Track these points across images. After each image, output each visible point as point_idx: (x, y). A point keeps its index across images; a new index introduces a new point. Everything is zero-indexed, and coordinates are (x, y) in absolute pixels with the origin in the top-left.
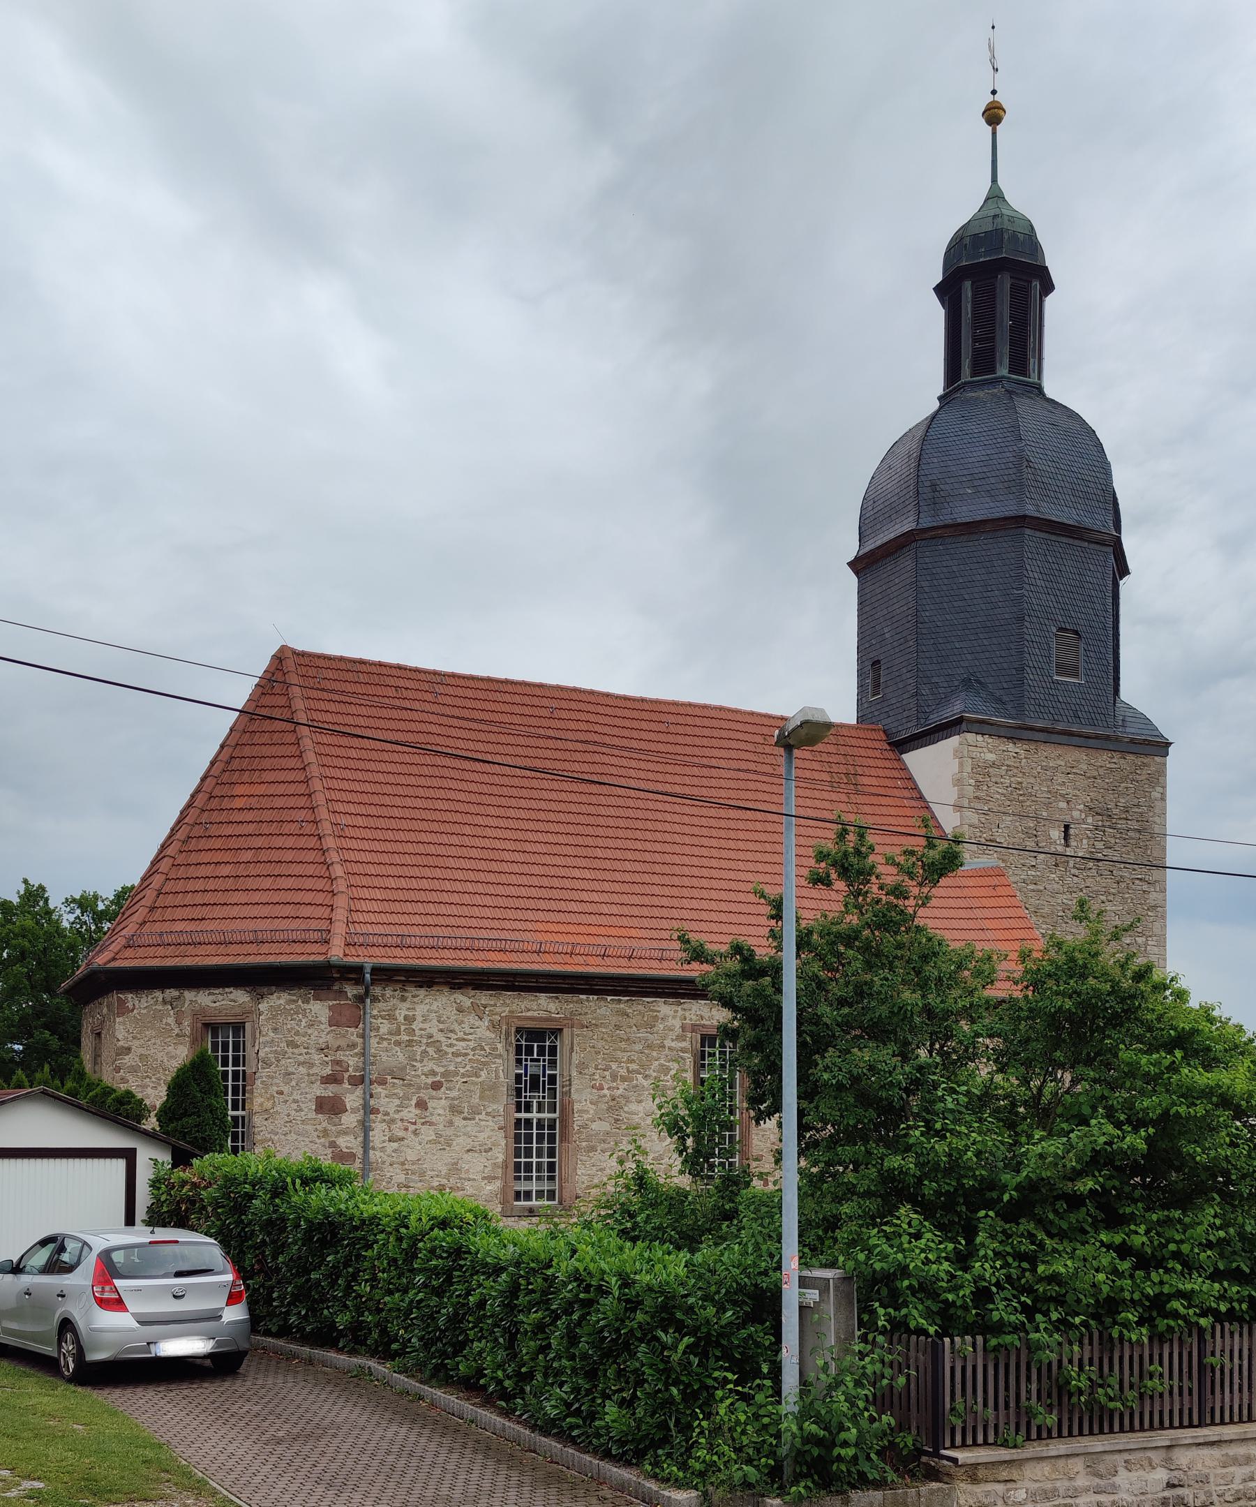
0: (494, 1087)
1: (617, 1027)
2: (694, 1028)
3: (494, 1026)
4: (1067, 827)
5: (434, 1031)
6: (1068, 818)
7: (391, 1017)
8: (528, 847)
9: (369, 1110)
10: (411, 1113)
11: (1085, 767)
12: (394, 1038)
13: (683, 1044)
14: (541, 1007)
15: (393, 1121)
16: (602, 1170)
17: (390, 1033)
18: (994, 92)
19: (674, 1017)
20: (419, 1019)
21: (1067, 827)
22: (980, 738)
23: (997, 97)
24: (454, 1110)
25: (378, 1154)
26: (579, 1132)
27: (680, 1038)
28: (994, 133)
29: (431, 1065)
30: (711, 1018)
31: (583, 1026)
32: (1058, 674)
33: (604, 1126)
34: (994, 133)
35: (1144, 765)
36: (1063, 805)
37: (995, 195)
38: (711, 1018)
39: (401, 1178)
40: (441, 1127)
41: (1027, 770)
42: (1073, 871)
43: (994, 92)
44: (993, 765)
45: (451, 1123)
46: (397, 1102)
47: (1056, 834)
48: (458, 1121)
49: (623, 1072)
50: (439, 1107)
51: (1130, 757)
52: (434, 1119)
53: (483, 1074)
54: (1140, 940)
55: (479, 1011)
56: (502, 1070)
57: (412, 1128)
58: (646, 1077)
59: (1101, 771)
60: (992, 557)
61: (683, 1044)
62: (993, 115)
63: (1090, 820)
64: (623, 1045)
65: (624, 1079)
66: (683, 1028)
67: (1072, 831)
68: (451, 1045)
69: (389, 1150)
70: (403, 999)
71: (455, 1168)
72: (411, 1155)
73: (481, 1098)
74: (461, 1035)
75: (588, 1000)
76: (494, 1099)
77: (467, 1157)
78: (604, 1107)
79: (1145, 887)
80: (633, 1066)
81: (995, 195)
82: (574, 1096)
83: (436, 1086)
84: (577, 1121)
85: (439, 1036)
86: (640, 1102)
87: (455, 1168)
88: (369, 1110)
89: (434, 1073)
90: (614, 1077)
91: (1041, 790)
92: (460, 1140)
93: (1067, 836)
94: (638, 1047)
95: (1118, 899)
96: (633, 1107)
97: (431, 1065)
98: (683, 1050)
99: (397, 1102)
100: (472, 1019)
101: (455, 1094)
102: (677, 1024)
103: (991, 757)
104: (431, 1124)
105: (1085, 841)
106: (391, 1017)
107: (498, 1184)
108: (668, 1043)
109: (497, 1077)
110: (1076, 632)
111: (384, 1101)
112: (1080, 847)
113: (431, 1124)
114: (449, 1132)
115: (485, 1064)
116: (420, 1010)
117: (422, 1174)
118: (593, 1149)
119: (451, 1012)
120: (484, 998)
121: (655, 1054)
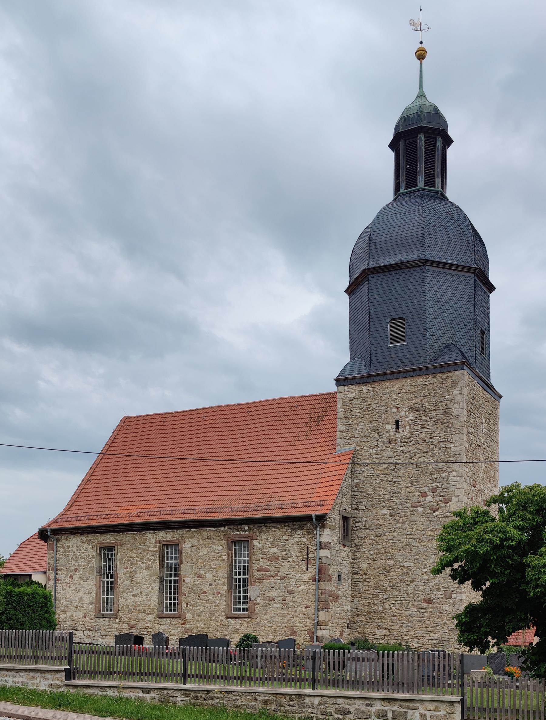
0: (92, 570)
1: (133, 544)
2: (160, 542)
3: (93, 547)
4: (397, 422)
5: (75, 550)
6: (398, 418)
7: (63, 547)
8: (189, 478)
9: (56, 579)
10: (68, 579)
11: (409, 388)
12: (64, 554)
13: (156, 549)
14: (108, 539)
15: (63, 583)
16: (127, 600)
17: (63, 552)
18: (421, 43)
19: (153, 538)
20: (71, 546)
21: (397, 422)
22: (346, 387)
23: (423, 45)
24: (81, 578)
25: (59, 595)
26: (119, 585)
27: (155, 547)
28: (421, 64)
29: (74, 563)
30: (167, 537)
31: (121, 545)
32: (391, 343)
33: (127, 583)
34: (421, 64)
35: (448, 377)
36: (395, 410)
37: (421, 95)
38: (167, 537)
39: (65, 603)
40: (77, 585)
41: (374, 397)
42: (400, 444)
43: (421, 43)
44: (354, 399)
45: (80, 583)
46: (64, 576)
47: (390, 427)
48: (82, 583)
49: (135, 562)
50: (76, 577)
51: (438, 376)
52: (75, 582)
53: (89, 565)
54: (443, 475)
55: (88, 541)
56: (95, 563)
57: (68, 585)
58: (143, 563)
59: (420, 388)
60: (417, 287)
61: (156, 549)
62: (421, 55)
63: (411, 415)
64: (135, 551)
65: (135, 564)
66: (156, 542)
67: (400, 423)
68: (80, 555)
69: (62, 593)
70: (67, 540)
71: (81, 599)
72: (68, 595)
73: (89, 574)
74: (83, 551)
75: (123, 535)
76: (92, 574)
77: (84, 595)
78: (128, 575)
79: (448, 445)
80: (138, 559)
81: (421, 95)
82: (118, 572)
83: (76, 570)
84: (119, 581)
85: (77, 552)
86: (140, 573)
87: (81, 599)
88: (56, 579)
89: (75, 565)
90: (131, 564)
91: (381, 406)
92: (82, 589)
93: (397, 427)
94: (140, 551)
95: (429, 454)
96: (138, 575)
97: (74, 563)
98: (156, 551)
99: (64, 576)
100: (86, 545)
101: (80, 573)
102: (154, 541)
103: (352, 395)
104: (74, 584)
105: (408, 427)
106: (63, 547)
107: (94, 605)
108: (150, 549)
109: (94, 566)
110: (402, 318)
111: (61, 576)
112: (405, 431)
113: (74, 584)
114: (79, 586)
115: (90, 561)
116: (72, 543)
117: (71, 602)
118: (124, 592)
119: (80, 543)
120: (90, 537)
121: (146, 554)
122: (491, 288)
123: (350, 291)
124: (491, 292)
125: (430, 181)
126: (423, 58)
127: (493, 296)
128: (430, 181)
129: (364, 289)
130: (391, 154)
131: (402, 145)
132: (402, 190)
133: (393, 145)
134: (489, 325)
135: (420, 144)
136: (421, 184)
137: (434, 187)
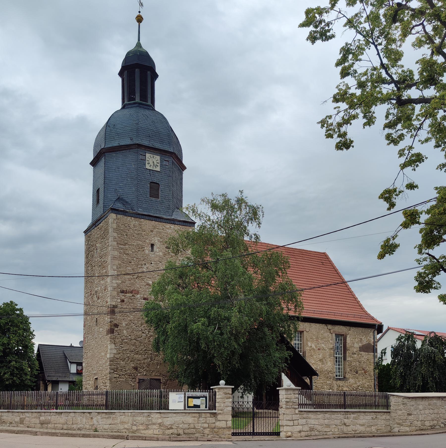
23: (141, 14)
28: (139, 40)
34: (139, 40)
37: (139, 45)
62: (140, 19)
81: (139, 45)
122: (184, 168)
123: (94, 163)
124: (183, 171)
125: (144, 97)
126: (141, 22)
127: (185, 173)
128: (144, 97)
129: (102, 164)
130: (120, 80)
131: (126, 72)
132: (126, 102)
133: (121, 74)
134: (182, 194)
135: (138, 74)
136: (138, 100)
137: (146, 102)
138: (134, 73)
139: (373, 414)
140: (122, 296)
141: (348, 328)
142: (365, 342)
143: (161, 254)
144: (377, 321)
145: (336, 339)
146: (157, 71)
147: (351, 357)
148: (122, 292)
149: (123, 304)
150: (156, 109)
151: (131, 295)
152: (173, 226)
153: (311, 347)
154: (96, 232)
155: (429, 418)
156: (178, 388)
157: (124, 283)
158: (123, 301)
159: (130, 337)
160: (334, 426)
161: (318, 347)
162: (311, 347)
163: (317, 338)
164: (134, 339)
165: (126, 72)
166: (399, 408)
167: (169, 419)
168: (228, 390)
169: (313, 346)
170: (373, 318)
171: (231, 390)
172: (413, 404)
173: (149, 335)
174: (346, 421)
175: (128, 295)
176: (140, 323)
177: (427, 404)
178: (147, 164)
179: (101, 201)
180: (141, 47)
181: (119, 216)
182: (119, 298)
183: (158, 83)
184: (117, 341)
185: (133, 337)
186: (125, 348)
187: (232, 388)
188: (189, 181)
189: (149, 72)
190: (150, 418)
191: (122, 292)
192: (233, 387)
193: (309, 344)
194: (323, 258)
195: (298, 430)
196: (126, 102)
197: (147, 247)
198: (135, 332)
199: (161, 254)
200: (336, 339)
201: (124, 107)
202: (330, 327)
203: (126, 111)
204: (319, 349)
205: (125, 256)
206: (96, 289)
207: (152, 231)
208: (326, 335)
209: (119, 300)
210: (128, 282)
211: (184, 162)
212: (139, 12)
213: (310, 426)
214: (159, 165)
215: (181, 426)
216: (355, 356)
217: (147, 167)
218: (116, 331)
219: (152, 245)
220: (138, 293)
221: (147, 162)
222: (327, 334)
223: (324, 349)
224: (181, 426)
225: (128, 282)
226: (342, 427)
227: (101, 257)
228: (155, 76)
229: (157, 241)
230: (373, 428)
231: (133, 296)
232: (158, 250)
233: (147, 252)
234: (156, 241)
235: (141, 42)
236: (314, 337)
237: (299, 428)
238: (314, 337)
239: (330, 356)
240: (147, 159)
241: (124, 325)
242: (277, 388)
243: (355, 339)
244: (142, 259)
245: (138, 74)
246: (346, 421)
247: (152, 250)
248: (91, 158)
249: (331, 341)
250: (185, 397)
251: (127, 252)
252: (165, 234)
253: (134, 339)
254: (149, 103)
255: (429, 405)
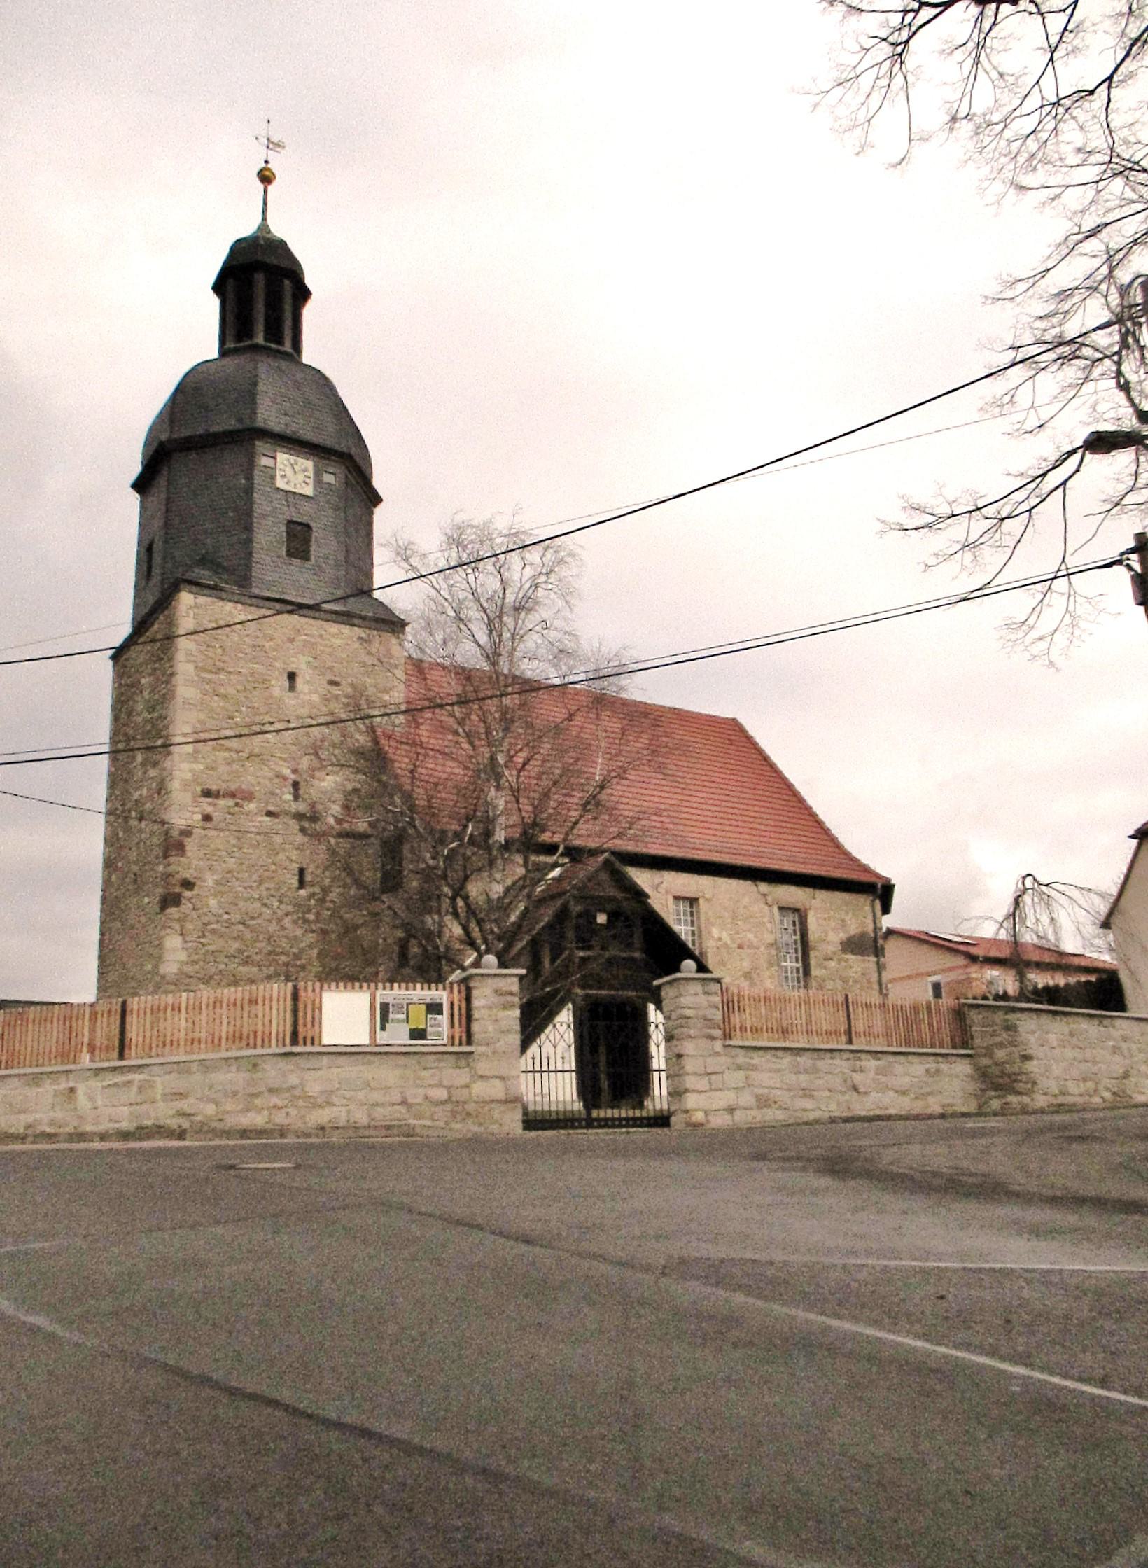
28: (264, 219)
34: (264, 219)
37: (264, 227)
62: (266, 177)
81: (264, 227)
122: (375, 499)
123: (141, 485)
125: (274, 332)
128: (274, 332)
129: (162, 481)
130: (214, 303)
133: (218, 288)
135: (261, 288)
136: (260, 339)
138: (250, 284)
139: (931, 1059)
140: (206, 805)
141: (809, 891)
142: (853, 929)
143: (315, 698)
144: (878, 876)
145: (782, 922)
146: (309, 281)
147: (820, 966)
148: (207, 793)
149: (208, 825)
150: (306, 359)
151: (231, 802)
152: (346, 630)
153: (720, 939)
154: (138, 655)
155: (1075, 1073)
156: (351, 978)
157: (213, 769)
158: (207, 818)
159: (226, 916)
160: (827, 1093)
161: (739, 941)
162: (720, 939)
163: (735, 917)
164: (239, 923)
165: (231, 283)
166: (998, 1039)
167: (320, 1073)
168: (510, 980)
169: (726, 937)
170: (866, 869)
171: (516, 980)
172: (1033, 1027)
173: (280, 913)
174: (858, 1078)
175: (222, 802)
176: (255, 877)
177: (1066, 1030)
178: (278, 477)
179: (156, 571)
180: (270, 232)
181: (202, 600)
182: (197, 809)
183: (309, 313)
184: (189, 926)
185: (236, 917)
186: (211, 948)
187: (521, 978)
188: (385, 522)
189: (287, 282)
190: (260, 1075)
191: (207, 793)
192: (524, 971)
193: (715, 932)
194: (732, 735)
195: (722, 1104)
196: (230, 345)
197: (277, 679)
198: (241, 904)
199: (315, 698)
200: (782, 922)
201: (224, 353)
202: (764, 887)
203: (226, 361)
204: (740, 947)
205: (217, 703)
206: (136, 796)
207: (291, 640)
208: (755, 908)
209: (199, 817)
210: (223, 769)
211: (377, 483)
212: (266, 162)
213: (760, 1091)
214: (311, 481)
215: (361, 1095)
216: (833, 964)
217: (280, 483)
218: (189, 899)
219: (292, 676)
220: (249, 797)
221: (279, 474)
222: (759, 908)
223: (751, 946)
224: (361, 1095)
225: (223, 769)
226: (847, 1097)
227: (152, 709)
228: (303, 294)
229: (303, 666)
230: (931, 1100)
231: (237, 805)
232: (306, 688)
233: (276, 692)
234: (301, 664)
235: (269, 222)
236: (726, 914)
237: (726, 1098)
238: (726, 914)
239: (770, 964)
240: (279, 466)
241: (210, 883)
242: (656, 983)
243: (832, 917)
244: (262, 710)
245: (261, 288)
246: (858, 1078)
247: (292, 688)
248: (136, 468)
249: (769, 925)
250: (372, 1006)
251: (222, 691)
252: (328, 650)
253: (239, 923)
254: (287, 347)
255: (1071, 1034)
